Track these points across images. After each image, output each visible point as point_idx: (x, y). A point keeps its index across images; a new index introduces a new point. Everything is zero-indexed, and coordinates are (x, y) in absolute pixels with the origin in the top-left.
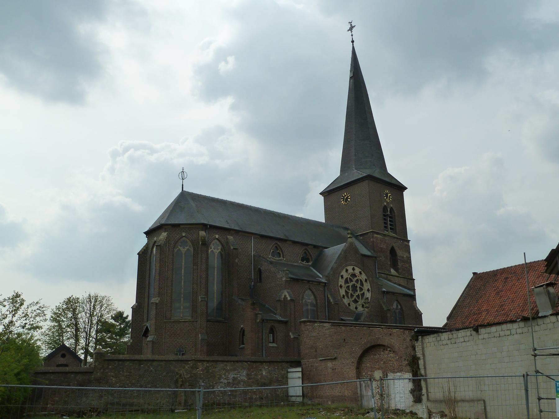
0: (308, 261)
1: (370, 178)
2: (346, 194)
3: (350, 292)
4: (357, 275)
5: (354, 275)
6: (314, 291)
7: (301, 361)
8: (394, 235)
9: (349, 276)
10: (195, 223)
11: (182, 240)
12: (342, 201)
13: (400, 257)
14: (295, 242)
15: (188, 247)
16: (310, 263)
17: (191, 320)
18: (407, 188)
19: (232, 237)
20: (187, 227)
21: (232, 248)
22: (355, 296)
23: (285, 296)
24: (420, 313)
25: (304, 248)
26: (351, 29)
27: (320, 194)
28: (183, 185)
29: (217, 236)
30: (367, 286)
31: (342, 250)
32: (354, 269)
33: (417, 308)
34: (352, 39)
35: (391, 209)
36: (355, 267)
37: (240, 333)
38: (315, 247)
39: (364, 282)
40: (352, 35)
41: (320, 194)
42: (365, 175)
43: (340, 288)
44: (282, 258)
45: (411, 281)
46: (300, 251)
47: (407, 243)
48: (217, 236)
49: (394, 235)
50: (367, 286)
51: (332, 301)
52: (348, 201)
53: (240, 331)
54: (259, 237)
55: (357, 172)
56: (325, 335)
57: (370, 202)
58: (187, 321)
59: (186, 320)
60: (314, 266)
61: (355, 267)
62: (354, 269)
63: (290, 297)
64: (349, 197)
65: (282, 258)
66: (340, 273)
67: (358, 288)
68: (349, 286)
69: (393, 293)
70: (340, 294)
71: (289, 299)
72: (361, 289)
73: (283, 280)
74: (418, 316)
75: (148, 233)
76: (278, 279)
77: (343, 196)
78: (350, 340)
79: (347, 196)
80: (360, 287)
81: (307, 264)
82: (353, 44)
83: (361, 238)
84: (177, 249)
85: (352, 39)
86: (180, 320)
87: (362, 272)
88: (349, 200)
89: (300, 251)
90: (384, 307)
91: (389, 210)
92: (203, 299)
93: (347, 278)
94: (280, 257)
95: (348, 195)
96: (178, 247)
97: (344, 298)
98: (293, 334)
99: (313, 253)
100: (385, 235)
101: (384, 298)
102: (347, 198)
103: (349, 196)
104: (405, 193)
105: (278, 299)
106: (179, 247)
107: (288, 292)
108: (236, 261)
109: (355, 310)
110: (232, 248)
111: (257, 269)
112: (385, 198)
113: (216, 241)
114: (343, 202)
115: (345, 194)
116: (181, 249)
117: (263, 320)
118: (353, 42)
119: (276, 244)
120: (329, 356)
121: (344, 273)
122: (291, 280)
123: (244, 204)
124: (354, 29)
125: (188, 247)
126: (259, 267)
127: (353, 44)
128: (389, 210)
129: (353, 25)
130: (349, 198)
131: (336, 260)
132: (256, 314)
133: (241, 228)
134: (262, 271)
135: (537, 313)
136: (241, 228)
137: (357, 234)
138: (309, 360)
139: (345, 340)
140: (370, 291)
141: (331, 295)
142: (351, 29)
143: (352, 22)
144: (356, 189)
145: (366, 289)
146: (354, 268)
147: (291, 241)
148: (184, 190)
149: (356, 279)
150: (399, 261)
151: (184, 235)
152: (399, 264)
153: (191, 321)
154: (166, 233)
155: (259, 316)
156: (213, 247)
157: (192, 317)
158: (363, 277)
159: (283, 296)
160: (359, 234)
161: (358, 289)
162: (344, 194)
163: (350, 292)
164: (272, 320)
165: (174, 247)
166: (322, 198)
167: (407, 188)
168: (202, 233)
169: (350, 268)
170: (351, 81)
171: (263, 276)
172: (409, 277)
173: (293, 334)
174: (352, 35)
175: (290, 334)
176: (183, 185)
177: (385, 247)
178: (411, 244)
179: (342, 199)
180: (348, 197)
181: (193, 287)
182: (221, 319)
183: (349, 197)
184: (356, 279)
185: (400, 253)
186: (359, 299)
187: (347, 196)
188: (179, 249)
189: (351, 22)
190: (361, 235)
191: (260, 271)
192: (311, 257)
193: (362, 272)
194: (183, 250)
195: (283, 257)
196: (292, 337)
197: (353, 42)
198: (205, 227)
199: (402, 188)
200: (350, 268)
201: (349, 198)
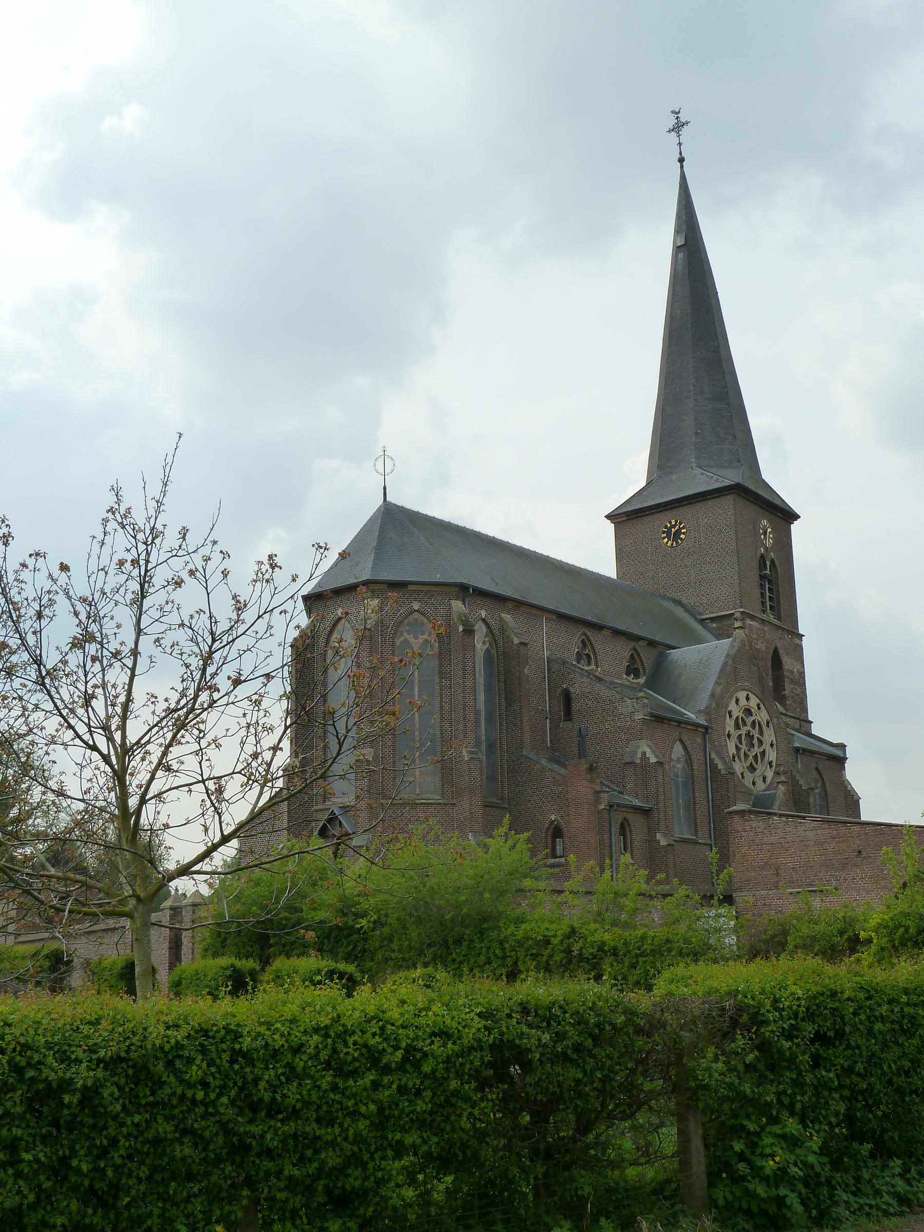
0: (637, 676)
1: (738, 490)
2: (676, 522)
3: (744, 748)
4: (753, 710)
5: (748, 712)
6: (688, 743)
7: (734, 895)
8: (776, 622)
9: (741, 714)
10: (441, 580)
11: (411, 618)
12: (664, 538)
13: (789, 671)
14: (617, 633)
15: (425, 636)
16: (642, 680)
17: (441, 801)
18: (800, 517)
19: (509, 616)
20: (416, 589)
21: (516, 641)
22: (751, 758)
23: (644, 753)
24: (855, 798)
25: (633, 644)
26: (678, 127)
27: (607, 517)
28: (385, 488)
29: (483, 614)
30: (769, 736)
31: (728, 655)
32: (748, 698)
33: (849, 788)
34: (681, 153)
35: (772, 561)
36: (750, 695)
37: (547, 832)
38: (652, 643)
39: (764, 727)
40: (680, 144)
41: (607, 517)
42: (727, 483)
43: (775, 742)
44: (593, 667)
45: (807, 725)
46: (624, 650)
47: (798, 641)
48: (416, 606)
49: (776, 622)
50: (769, 736)
51: (720, 766)
52: (681, 539)
53: (548, 829)
54: (554, 617)
55: (702, 474)
56: (803, 841)
57: (737, 545)
58: (431, 804)
59: (429, 801)
60: (648, 685)
61: (750, 695)
62: (748, 698)
63: (656, 756)
64: (683, 531)
65: (593, 667)
66: (727, 707)
67: (756, 739)
68: (740, 735)
69: (812, 753)
70: (728, 752)
71: (653, 760)
72: (761, 743)
73: (636, 718)
74: (852, 801)
75: (312, 601)
76: (622, 716)
77: (666, 527)
78: (875, 853)
79: (677, 527)
80: (758, 739)
81: (635, 681)
82: (682, 167)
83: (714, 625)
84: (402, 638)
85: (681, 153)
86: (417, 801)
87: (762, 706)
88: (683, 536)
89: (624, 650)
90: (801, 782)
91: (768, 563)
92: (474, 756)
93: (737, 718)
94: (589, 664)
95: (680, 524)
96: (402, 635)
97: (734, 761)
98: (665, 836)
99: (648, 657)
100: (763, 622)
101: (797, 762)
102: (678, 532)
103: (683, 528)
104: (795, 527)
105: (628, 760)
106: (405, 634)
107: (649, 746)
108: (526, 671)
109: (752, 787)
110: (516, 641)
111: (559, 691)
112: (762, 537)
113: (416, 615)
114: (666, 540)
115: (673, 523)
116: (411, 639)
117: (611, 806)
118: (681, 160)
119: (585, 634)
120: (814, 885)
121: (732, 706)
122: (653, 719)
123: (497, 539)
124: (684, 131)
125: (425, 636)
126: (565, 686)
127: (682, 167)
128: (768, 563)
129: (683, 120)
130: (684, 533)
131: (719, 678)
132: (598, 793)
133: (523, 597)
134: (574, 696)
135: (278, 799)
136: (523, 597)
137: (704, 617)
138: (757, 893)
139: (860, 852)
140: (775, 747)
141: (717, 753)
142: (678, 127)
143: (679, 112)
144: (703, 513)
145: (769, 744)
146: (748, 695)
147: (610, 628)
148: (388, 499)
149: (752, 719)
150: (786, 680)
151: (416, 606)
152: (787, 687)
153: (440, 804)
154: (377, 602)
155: (605, 796)
156: (411, 636)
157: (443, 794)
158: (763, 716)
159: (639, 755)
160: (708, 616)
161: (755, 741)
162: (670, 523)
163: (744, 748)
164: (626, 806)
165: (395, 635)
166: (610, 527)
167: (800, 517)
168: (457, 606)
169: (742, 695)
170: (681, 255)
171: (575, 706)
172: (802, 717)
173: (665, 835)
174: (680, 144)
175: (659, 836)
176: (385, 488)
177: (763, 649)
178: (805, 642)
179: (664, 532)
180: (680, 529)
181: (441, 727)
182: (494, 800)
183: (683, 531)
184: (752, 719)
185: (788, 663)
186: (757, 763)
187: (677, 527)
188: (406, 640)
189: (677, 111)
190: (713, 619)
191: (567, 697)
192: (644, 667)
193: (762, 706)
194: (416, 643)
195: (597, 666)
196: (663, 843)
197: (681, 160)
198: (464, 591)
199: (790, 516)
200: (742, 695)
201: (684, 533)
